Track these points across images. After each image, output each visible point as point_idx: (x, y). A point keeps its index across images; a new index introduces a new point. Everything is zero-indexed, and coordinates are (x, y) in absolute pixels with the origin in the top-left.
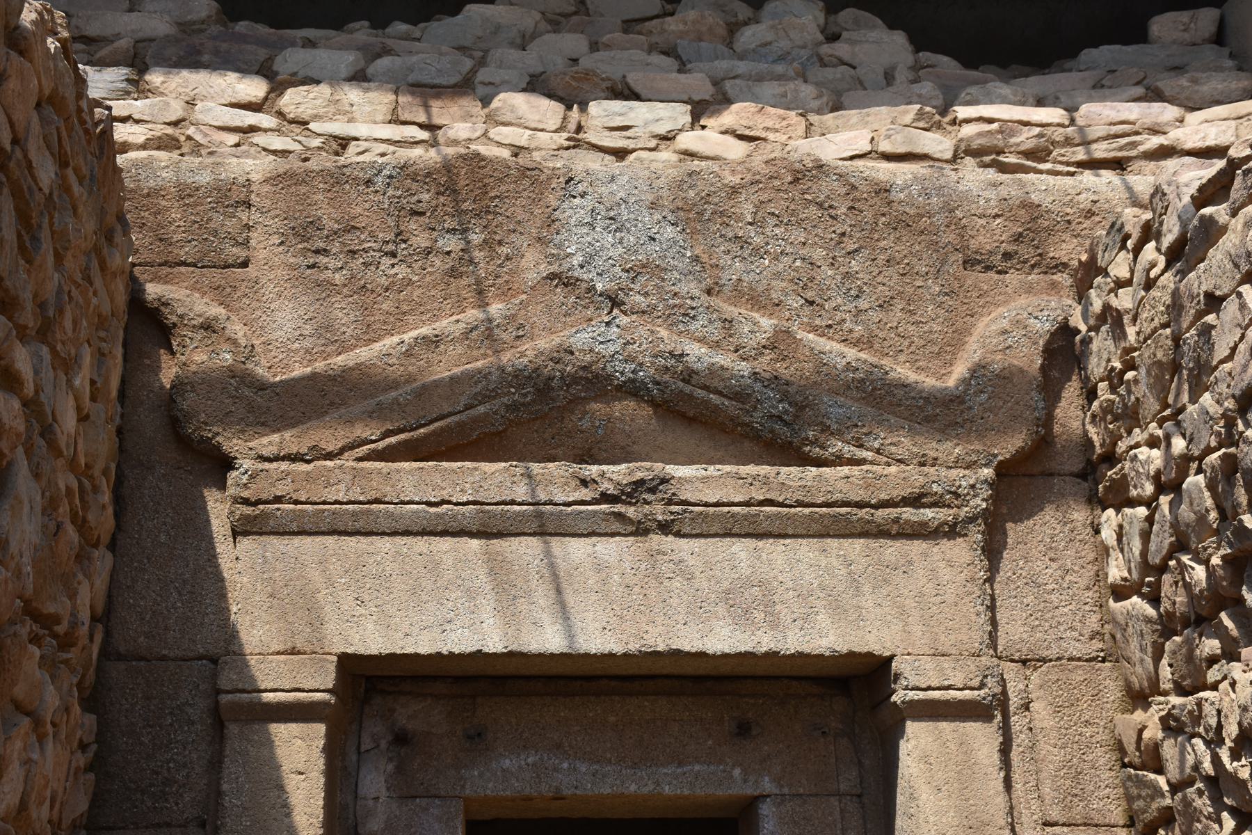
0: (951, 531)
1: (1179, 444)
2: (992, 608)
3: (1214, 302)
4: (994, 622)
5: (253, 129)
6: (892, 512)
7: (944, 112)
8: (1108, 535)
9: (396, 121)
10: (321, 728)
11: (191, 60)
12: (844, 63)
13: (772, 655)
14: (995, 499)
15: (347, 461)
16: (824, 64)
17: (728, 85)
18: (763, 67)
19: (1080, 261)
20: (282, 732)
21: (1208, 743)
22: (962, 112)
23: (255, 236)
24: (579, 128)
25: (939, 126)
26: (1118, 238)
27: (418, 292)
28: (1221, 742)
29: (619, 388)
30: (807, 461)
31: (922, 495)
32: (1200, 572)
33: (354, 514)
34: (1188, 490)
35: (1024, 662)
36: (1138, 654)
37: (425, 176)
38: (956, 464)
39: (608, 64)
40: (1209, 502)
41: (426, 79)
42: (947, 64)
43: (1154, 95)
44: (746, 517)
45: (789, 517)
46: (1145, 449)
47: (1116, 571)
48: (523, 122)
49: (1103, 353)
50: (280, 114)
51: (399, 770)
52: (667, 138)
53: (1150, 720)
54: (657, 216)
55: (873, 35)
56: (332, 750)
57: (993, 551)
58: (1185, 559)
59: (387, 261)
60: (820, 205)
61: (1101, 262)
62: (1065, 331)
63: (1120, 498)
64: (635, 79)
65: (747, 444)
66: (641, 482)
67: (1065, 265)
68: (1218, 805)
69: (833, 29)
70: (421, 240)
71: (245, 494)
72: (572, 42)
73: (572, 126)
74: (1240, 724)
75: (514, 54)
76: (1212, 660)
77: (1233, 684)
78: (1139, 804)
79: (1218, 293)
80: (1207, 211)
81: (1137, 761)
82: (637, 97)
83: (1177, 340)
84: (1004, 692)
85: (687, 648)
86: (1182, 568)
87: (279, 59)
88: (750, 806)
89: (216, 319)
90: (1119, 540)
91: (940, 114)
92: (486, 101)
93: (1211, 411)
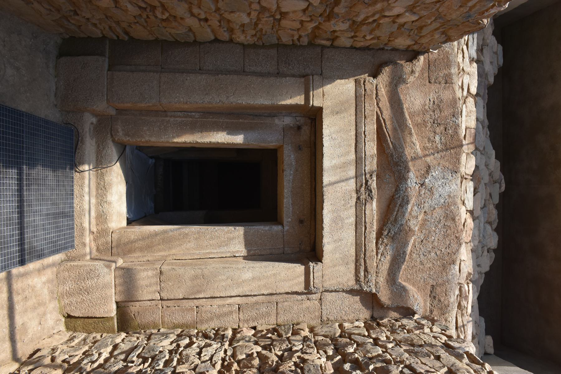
0: (357, 280)
1: (390, 346)
2: (336, 291)
3: (438, 358)
4: (332, 291)
5: (463, 89)
6: (363, 264)
8: (357, 324)
10: (303, 103)
11: (480, 75)
12: (483, 253)
13: (322, 228)
14: (366, 293)
15: (376, 109)
16: (483, 247)
17: (477, 221)
19: (434, 318)
21: (301, 349)
22: (471, 285)
23: (438, 85)
24: (466, 179)
25: (467, 279)
26: (444, 328)
27: (423, 129)
28: (302, 353)
29: (398, 186)
30: (377, 239)
31: (368, 272)
32: (352, 350)
33: (362, 111)
34: (376, 348)
35: (321, 299)
36: (324, 330)
37: (456, 133)
38: (377, 283)
39: (482, 187)
40: (374, 354)
41: (477, 137)
42: (481, 281)
44: (362, 222)
45: (361, 234)
46: (385, 335)
47: (346, 325)
48: (468, 164)
49: (409, 323)
50: (467, 97)
51: (291, 127)
52: (464, 203)
53: (306, 333)
54: (447, 197)
55: (489, 262)
57: (352, 292)
58: (355, 346)
59: (432, 121)
60: (450, 244)
61: (436, 323)
62: (414, 313)
63: (368, 327)
64: (479, 195)
65: (382, 223)
66: (371, 192)
67: (432, 313)
68: (285, 350)
69: (490, 251)
70: (438, 130)
71: (367, 81)
72: (486, 179)
73: (466, 177)
74: (308, 359)
75: (484, 162)
76: (326, 352)
77: (319, 358)
78: (283, 328)
79: (441, 359)
80: (465, 356)
81: (295, 328)
82: (474, 195)
83: (421, 346)
84: (312, 293)
85: (324, 204)
86: (352, 345)
87: (480, 98)
88: (281, 223)
89: (415, 74)
90: (356, 327)
91: (470, 279)
92: (472, 153)
93: (403, 356)
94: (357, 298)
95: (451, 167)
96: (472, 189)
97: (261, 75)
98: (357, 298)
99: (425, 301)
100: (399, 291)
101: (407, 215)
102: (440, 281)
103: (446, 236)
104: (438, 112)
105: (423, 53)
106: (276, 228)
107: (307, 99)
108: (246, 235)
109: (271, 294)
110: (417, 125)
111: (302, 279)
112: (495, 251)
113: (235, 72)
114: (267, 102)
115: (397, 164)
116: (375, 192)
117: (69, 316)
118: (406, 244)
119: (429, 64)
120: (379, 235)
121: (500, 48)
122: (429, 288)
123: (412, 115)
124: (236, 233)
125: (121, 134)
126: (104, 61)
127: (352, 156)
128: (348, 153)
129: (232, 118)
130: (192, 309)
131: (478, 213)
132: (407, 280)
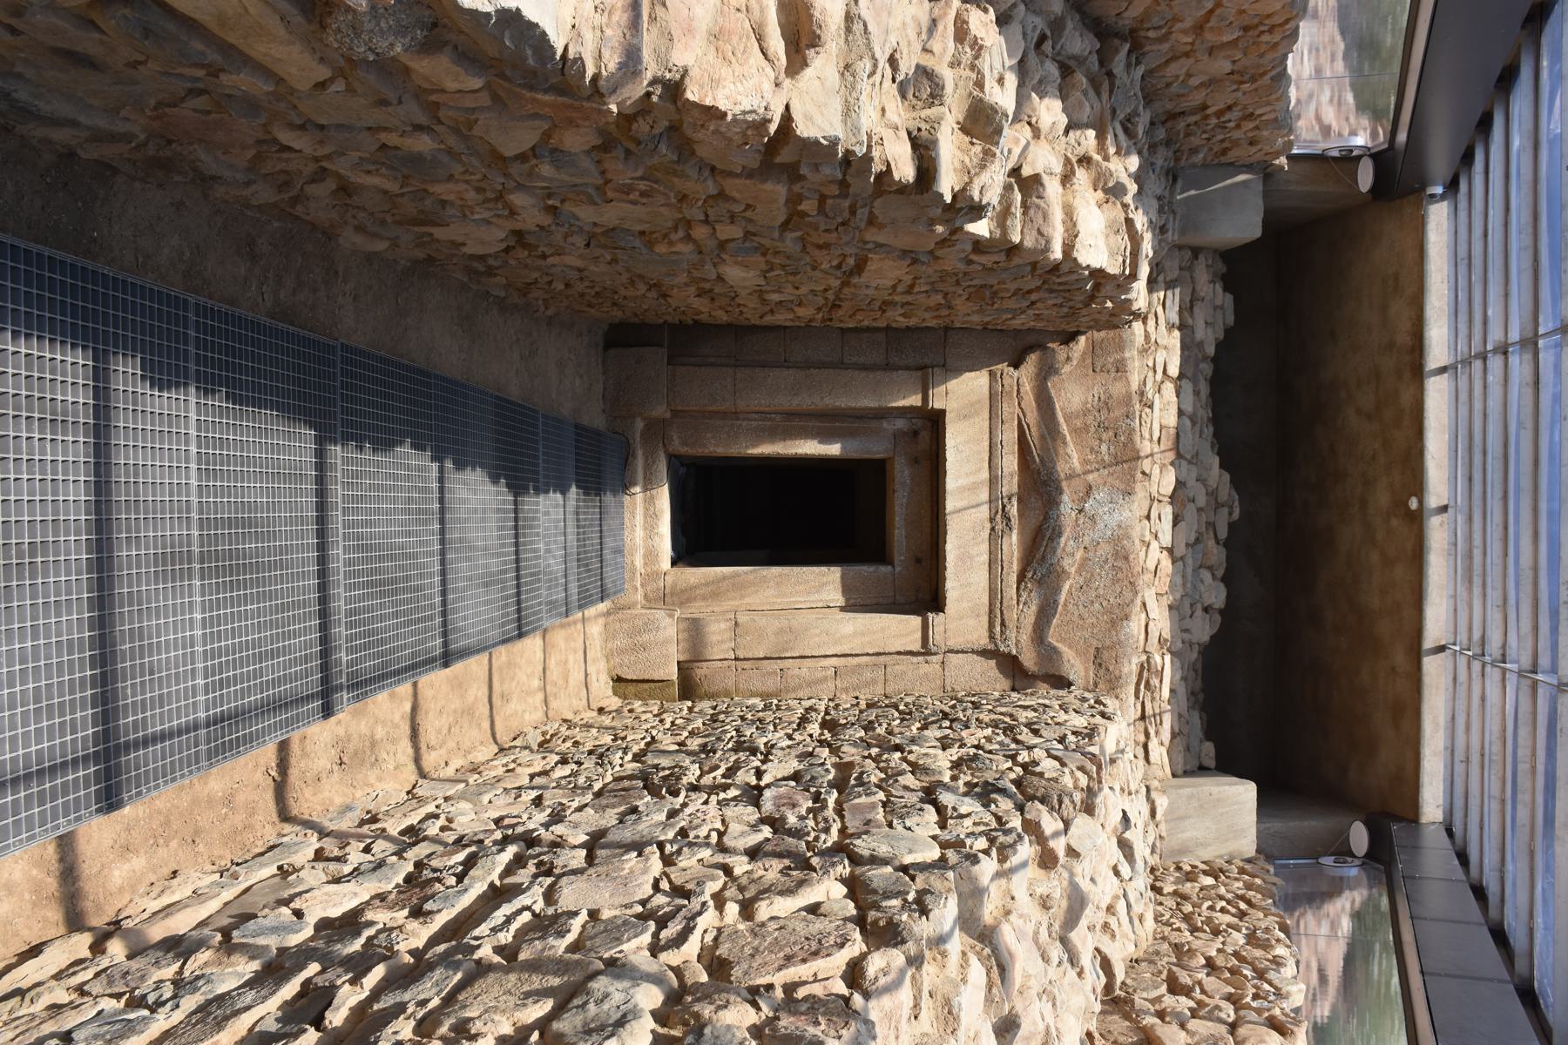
0: (992, 637)
9: (1162, 428)
13: (945, 568)
15: (1017, 410)
16: (1192, 605)
18: (1189, 578)
20: (920, 396)
22: (1168, 658)
38: (1018, 642)
43: (1174, 735)
56: (912, 408)
57: (984, 653)
62: (1070, 684)
64: (1182, 525)
70: (1104, 436)
72: (1202, 500)
75: (1194, 475)
88: (891, 563)
92: (1172, 464)
94: (993, 663)
95: (1122, 487)
96: (1170, 517)
97: (865, 368)
98: (993, 663)
99: (1087, 670)
100: (1049, 654)
101: (1059, 551)
102: (1108, 643)
103: (1115, 581)
104: (1104, 411)
106: (884, 569)
107: (925, 399)
108: (843, 578)
110: (1075, 431)
111: (919, 635)
112: (1221, 612)
115: (1045, 484)
116: (1015, 522)
117: (618, 680)
118: (1057, 590)
119: (1093, 347)
120: (1021, 578)
121: (1229, 298)
122: (1092, 651)
123: (1067, 418)
125: (676, 442)
126: (662, 353)
127: (985, 475)
129: (825, 423)
130: (775, 673)
131: (1181, 550)
132: (1062, 640)
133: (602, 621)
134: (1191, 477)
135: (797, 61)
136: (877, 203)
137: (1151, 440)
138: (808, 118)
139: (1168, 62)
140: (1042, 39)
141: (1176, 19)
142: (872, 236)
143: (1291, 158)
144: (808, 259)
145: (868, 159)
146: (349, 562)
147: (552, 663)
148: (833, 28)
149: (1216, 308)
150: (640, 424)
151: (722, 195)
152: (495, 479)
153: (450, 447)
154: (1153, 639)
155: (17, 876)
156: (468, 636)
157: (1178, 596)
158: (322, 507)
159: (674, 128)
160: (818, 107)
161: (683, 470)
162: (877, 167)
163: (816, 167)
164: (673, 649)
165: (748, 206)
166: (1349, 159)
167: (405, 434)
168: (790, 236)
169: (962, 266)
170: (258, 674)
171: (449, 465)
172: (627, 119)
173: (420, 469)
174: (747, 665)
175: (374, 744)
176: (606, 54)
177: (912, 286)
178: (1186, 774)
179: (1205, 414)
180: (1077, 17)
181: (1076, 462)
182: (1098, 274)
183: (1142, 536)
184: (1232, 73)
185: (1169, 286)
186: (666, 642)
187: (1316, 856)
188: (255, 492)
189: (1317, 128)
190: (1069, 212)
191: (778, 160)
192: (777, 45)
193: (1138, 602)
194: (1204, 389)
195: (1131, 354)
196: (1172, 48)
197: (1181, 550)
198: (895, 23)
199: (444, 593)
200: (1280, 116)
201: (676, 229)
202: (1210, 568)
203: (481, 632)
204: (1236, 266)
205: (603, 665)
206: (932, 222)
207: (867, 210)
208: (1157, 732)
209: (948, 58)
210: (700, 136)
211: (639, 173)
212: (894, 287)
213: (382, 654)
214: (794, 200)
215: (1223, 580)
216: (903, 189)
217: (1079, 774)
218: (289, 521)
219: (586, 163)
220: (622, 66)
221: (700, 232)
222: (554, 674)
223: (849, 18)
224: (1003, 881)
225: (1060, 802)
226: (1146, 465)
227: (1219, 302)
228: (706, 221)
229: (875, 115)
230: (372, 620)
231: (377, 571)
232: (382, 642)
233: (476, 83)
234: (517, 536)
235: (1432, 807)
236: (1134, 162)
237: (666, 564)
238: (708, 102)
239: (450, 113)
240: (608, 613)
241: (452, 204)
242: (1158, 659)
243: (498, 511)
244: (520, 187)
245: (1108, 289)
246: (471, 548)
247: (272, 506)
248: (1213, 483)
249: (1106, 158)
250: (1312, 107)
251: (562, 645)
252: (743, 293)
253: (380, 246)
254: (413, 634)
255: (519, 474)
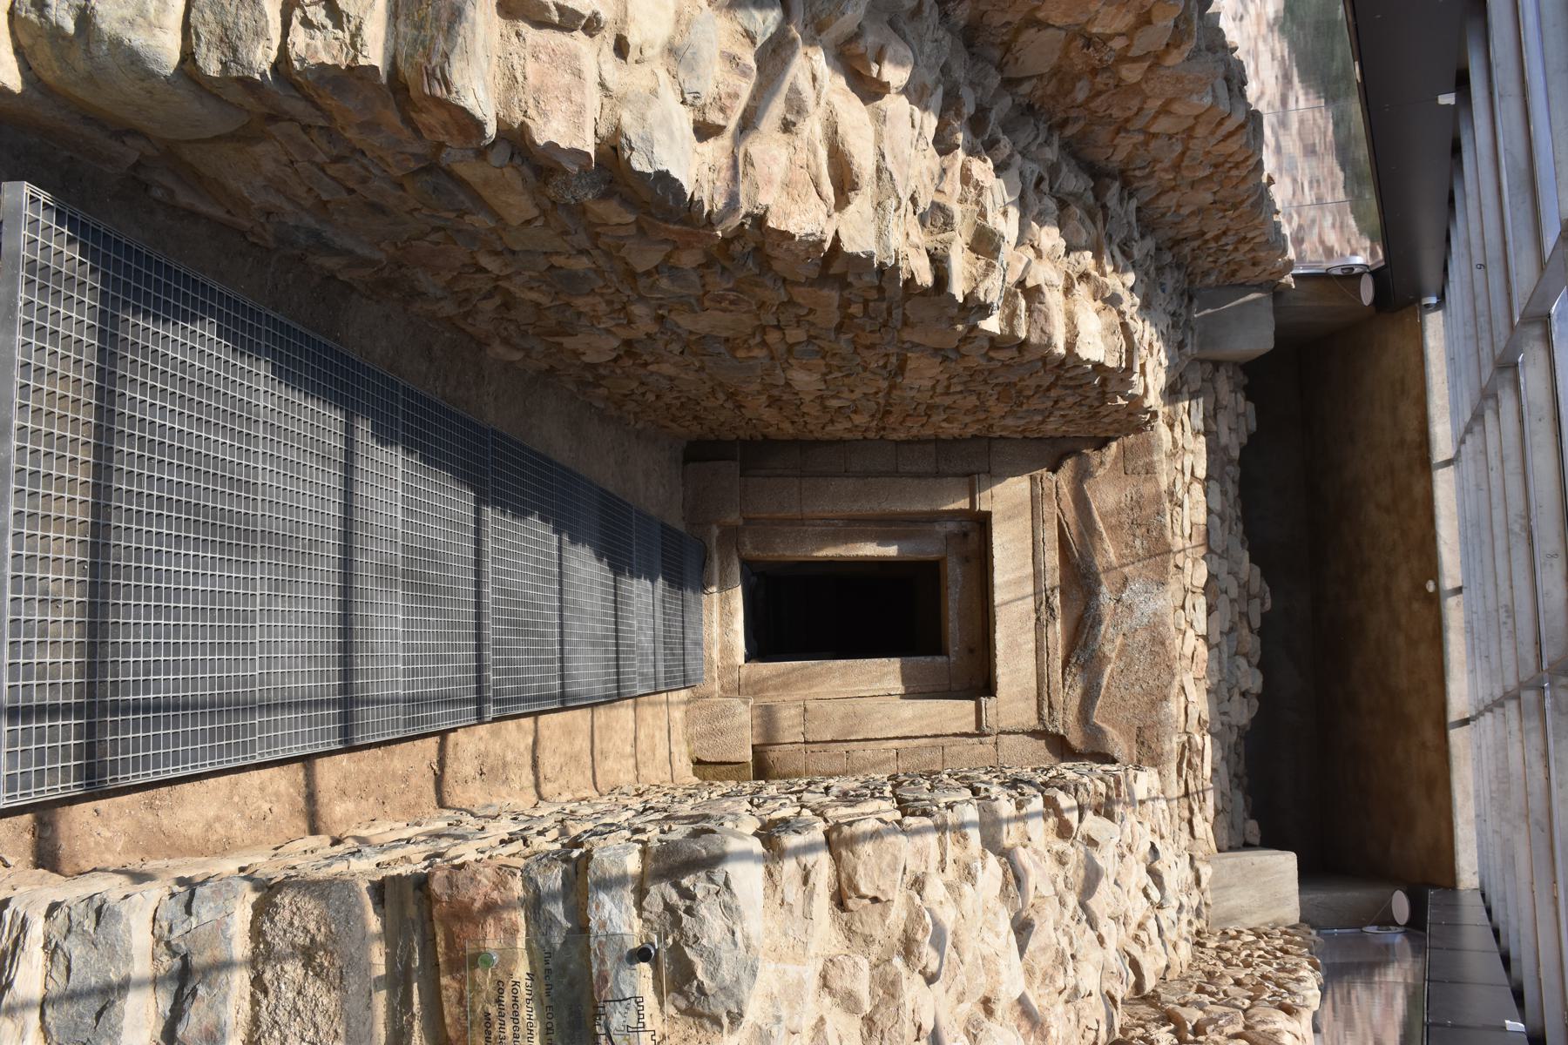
0: (1040, 719)
7: (1209, 731)
9: (1192, 525)
15: (1057, 510)
22: (1208, 738)
43: (1217, 812)
56: (961, 512)
57: (1034, 734)
64: (1216, 614)
70: (1138, 532)
72: (1234, 592)
75: (1225, 569)
88: (947, 655)
92: (1204, 558)
97: (918, 476)
99: (1130, 748)
100: (1094, 732)
103: (1153, 665)
104: (1137, 510)
105: (1115, 439)
106: (939, 659)
107: (973, 502)
108: (902, 668)
109: (936, 736)
110: (1110, 528)
111: (973, 718)
112: (1259, 697)
113: (887, 474)
114: (926, 508)
115: (1084, 576)
116: (1058, 612)
118: (1100, 674)
119: (1124, 453)
121: (1251, 406)
122: (1135, 730)
123: (1103, 517)
124: (894, 664)
127: (1030, 570)
128: (1024, 565)
129: (882, 527)
131: (1216, 638)
132: (1106, 721)
133: (683, 708)
134: (1222, 569)
135: (842, 202)
136: (908, 305)
137: (1183, 536)
138: (851, 239)
139: (1158, 196)
140: (1040, 180)
141: (1156, 161)
142: (906, 335)
143: (1295, 277)
144: (859, 360)
145: (896, 268)
146: (496, 601)
147: (642, 735)
148: (867, 177)
149: (1238, 415)
150: (716, 531)
151: (791, 302)
152: (599, 558)
153: (567, 524)
154: (1193, 720)
155: (282, 789)
156: (579, 684)
157: (1215, 680)
158: (478, 552)
159: (758, 249)
160: (858, 231)
161: (754, 579)
162: (903, 275)
163: (859, 276)
164: (748, 733)
165: (811, 311)
166: (1350, 277)
167: (535, 507)
168: (844, 337)
169: (983, 362)
170: (436, 671)
171: (566, 538)
172: (727, 241)
173: (545, 537)
174: (816, 747)
175: (505, 765)
176: (717, 198)
177: (948, 387)
178: (1231, 849)
179: (1234, 512)
180: (1073, 162)
181: (1112, 556)
182: (1099, 366)
183: (1178, 624)
184: (1215, 202)
185: (1193, 396)
186: (741, 727)
187: (1360, 925)
188: (437, 533)
189: (1321, 250)
190: (1071, 319)
191: (832, 271)
192: (828, 189)
193: (1176, 684)
194: (1232, 490)
195: (1159, 457)
196: (1160, 184)
197: (1216, 638)
198: (913, 172)
199: (562, 643)
200: (1272, 238)
201: (754, 335)
202: (1245, 655)
203: (589, 684)
204: (1256, 377)
205: (684, 748)
206: (952, 324)
207: (900, 311)
208: (1201, 809)
209: (957, 196)
210: (775, 253)
211: (730, 285)
212: (934, 387)
213: (516, 681)
214: (845, 304)
215: (1258, 666)
216: (924, 292)
217: (1098, 782)
218: (457, 559)
219: (694, 277)
220: (727, 205)
221: (773, 337)
222: (643, 745)
223: (879, 170)
224: (1021, 824)
225: (1076, 790)
226: (1179, 559)
227: (1241, 409)
228: (778, 327)
229: (901, 239)
230: (510, 651)
231: (514, 613)
232: (517, 671)
233: (631, 218)
234: (616, 609)
235: (1468, 873)
236: (1130, 278)
237: (740, 659)
238: (783, 228)
239: (607, 240)
240: (688, 702)
241: (585, 314)
242: (1198, 738)
243: (602, 584)
244: (642, 299)
245: (1113, 386)
246: (582, 611)
247: (447, 545)
248: (1244, 576)
249: (1104, 274)
250: (1316, 231)
251: (650, 720)
252: (807, 399)
253: (517, 356)
254: (540, 670)
255: (620, 558)
